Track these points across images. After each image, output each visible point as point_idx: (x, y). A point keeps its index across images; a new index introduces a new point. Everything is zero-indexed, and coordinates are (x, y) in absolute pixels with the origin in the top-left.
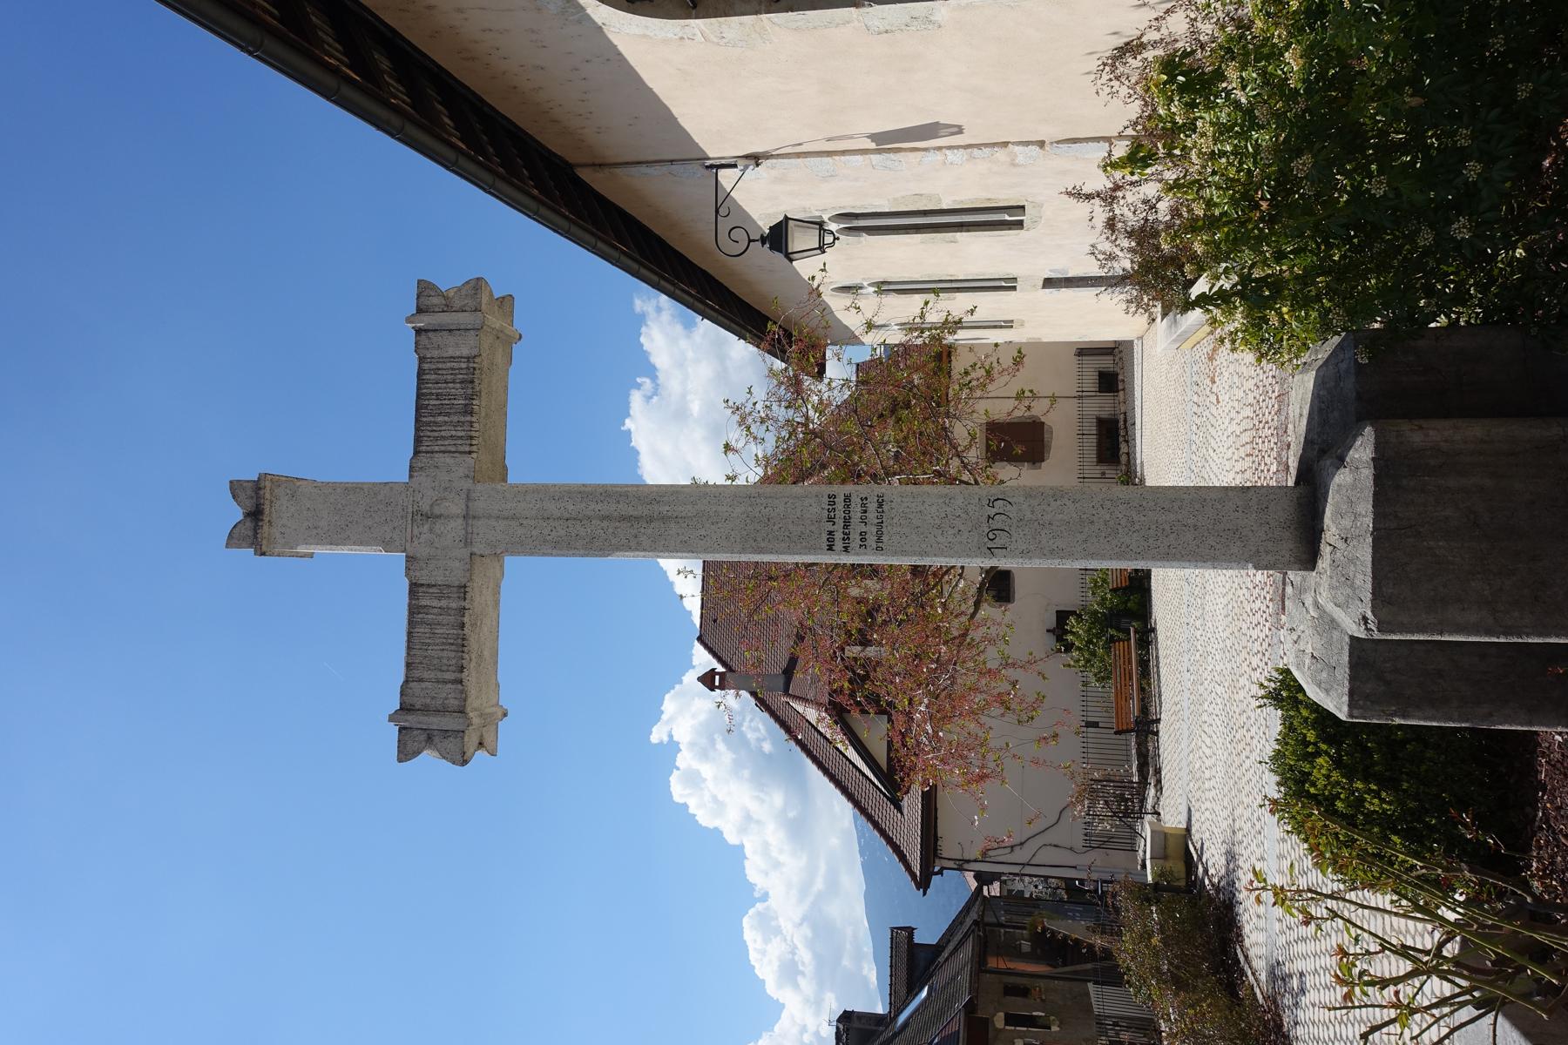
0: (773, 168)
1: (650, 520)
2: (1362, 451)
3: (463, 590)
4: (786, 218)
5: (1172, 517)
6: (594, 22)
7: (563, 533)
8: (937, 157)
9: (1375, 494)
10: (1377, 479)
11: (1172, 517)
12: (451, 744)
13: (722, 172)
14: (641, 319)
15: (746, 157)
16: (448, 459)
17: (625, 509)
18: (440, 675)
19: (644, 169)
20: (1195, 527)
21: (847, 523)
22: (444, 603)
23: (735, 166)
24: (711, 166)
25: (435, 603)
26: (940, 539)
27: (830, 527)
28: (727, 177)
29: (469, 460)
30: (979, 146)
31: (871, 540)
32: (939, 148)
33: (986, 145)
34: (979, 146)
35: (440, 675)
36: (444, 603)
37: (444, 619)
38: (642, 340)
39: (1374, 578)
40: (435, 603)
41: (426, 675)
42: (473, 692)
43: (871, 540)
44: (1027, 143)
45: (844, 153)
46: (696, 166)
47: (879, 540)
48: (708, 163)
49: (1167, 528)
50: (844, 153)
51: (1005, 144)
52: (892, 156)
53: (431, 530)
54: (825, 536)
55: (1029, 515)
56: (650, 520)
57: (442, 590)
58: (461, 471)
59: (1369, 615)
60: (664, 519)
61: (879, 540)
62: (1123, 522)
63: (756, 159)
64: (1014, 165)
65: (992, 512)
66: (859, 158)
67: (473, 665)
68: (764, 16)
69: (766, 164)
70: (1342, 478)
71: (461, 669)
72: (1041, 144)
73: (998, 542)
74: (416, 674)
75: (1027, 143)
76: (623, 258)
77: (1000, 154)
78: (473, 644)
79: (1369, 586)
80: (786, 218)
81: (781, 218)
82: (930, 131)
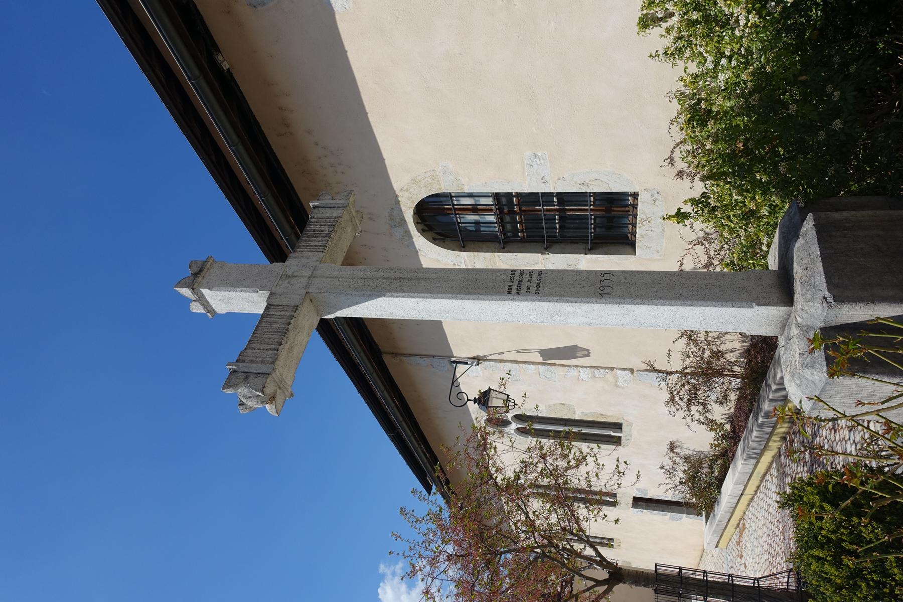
0: (486, 368)
1: (411, 279)
2: (808, 226)
3: (296, 308)
4: (490, 389)
5: (706, 282)
6: (415, 248)
7: (360, 284)
8: (573, 372)
9: (819, 240)
10: (818, 233)
11: (706, 282)
12: (259, 381)
13: (459, 366)
14: (382, 577)
15: (473, 358)
16: (310, 254)
17: (398, 275)
18: (266, 346)
19: (418, 359)
20: (720, 286)
21: (520, 282)
22: (283, 313)
23: (466, 363)
24: (454, 362)
25: (278, 313)
26: (572, 289)
27: (510, 283)
28: (461, 368)
29: (321, 254)
30: (598, 368)
31: (533, 290)
32: (577, 366)
33: (602, 368)
34: (598, 368)
35: (266, 346)
36: (283, 313)
37: (280, 321)
38: (379, 591)
39: (826, 276)
40: (278, 313)
41: (258, 346)
42: (280, 363)
43: (533, 290)
44: (624, 369)
45: (525, 363)
46: (445, 362)
47: (538, 289)
48: (453, 359)
49: (703, 286)
50: (525, 363)
51: (612, 368)
52: (550, 367)
53: (289, 283)
54: (507, 287)
55: (623, 280)
56: (411, 279)
57: (283, 307)
58: (315, 259)
59: (827, 294)
60: (418, 279)
61: (538, 289)
62: (678, 283)
63: (478, 360)
64: (617, 386)
65: (603, 279)
66: (532, 366)
67: (287, 346)
68: (497, 254)
69: (484, 364)
70: (800, 243)
71: (280, 344)
72: (632, 371)
73: (605, 292)
74: (253, 345)
75: (624, 369)
76: (395, 409)
77: (609, 375)
78: (291, 334)
79: (824, 280)
80: (490, 389)
81: (487, 389)
82: (571, 352)
